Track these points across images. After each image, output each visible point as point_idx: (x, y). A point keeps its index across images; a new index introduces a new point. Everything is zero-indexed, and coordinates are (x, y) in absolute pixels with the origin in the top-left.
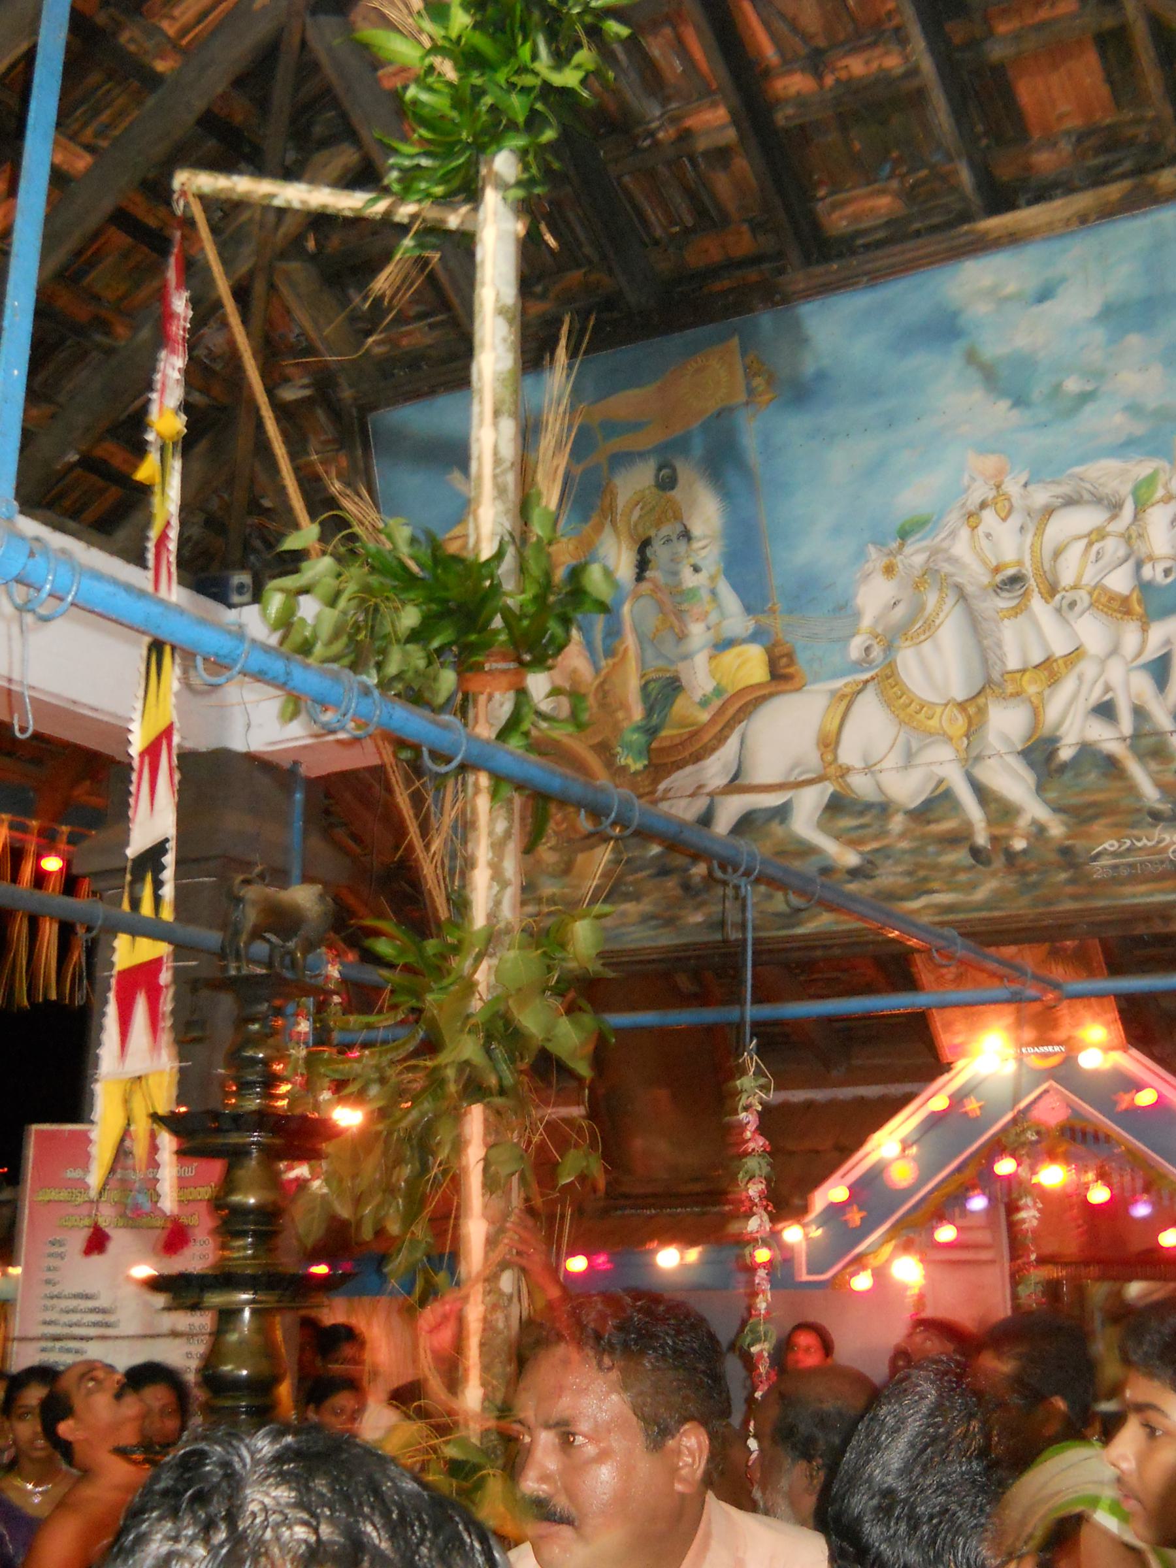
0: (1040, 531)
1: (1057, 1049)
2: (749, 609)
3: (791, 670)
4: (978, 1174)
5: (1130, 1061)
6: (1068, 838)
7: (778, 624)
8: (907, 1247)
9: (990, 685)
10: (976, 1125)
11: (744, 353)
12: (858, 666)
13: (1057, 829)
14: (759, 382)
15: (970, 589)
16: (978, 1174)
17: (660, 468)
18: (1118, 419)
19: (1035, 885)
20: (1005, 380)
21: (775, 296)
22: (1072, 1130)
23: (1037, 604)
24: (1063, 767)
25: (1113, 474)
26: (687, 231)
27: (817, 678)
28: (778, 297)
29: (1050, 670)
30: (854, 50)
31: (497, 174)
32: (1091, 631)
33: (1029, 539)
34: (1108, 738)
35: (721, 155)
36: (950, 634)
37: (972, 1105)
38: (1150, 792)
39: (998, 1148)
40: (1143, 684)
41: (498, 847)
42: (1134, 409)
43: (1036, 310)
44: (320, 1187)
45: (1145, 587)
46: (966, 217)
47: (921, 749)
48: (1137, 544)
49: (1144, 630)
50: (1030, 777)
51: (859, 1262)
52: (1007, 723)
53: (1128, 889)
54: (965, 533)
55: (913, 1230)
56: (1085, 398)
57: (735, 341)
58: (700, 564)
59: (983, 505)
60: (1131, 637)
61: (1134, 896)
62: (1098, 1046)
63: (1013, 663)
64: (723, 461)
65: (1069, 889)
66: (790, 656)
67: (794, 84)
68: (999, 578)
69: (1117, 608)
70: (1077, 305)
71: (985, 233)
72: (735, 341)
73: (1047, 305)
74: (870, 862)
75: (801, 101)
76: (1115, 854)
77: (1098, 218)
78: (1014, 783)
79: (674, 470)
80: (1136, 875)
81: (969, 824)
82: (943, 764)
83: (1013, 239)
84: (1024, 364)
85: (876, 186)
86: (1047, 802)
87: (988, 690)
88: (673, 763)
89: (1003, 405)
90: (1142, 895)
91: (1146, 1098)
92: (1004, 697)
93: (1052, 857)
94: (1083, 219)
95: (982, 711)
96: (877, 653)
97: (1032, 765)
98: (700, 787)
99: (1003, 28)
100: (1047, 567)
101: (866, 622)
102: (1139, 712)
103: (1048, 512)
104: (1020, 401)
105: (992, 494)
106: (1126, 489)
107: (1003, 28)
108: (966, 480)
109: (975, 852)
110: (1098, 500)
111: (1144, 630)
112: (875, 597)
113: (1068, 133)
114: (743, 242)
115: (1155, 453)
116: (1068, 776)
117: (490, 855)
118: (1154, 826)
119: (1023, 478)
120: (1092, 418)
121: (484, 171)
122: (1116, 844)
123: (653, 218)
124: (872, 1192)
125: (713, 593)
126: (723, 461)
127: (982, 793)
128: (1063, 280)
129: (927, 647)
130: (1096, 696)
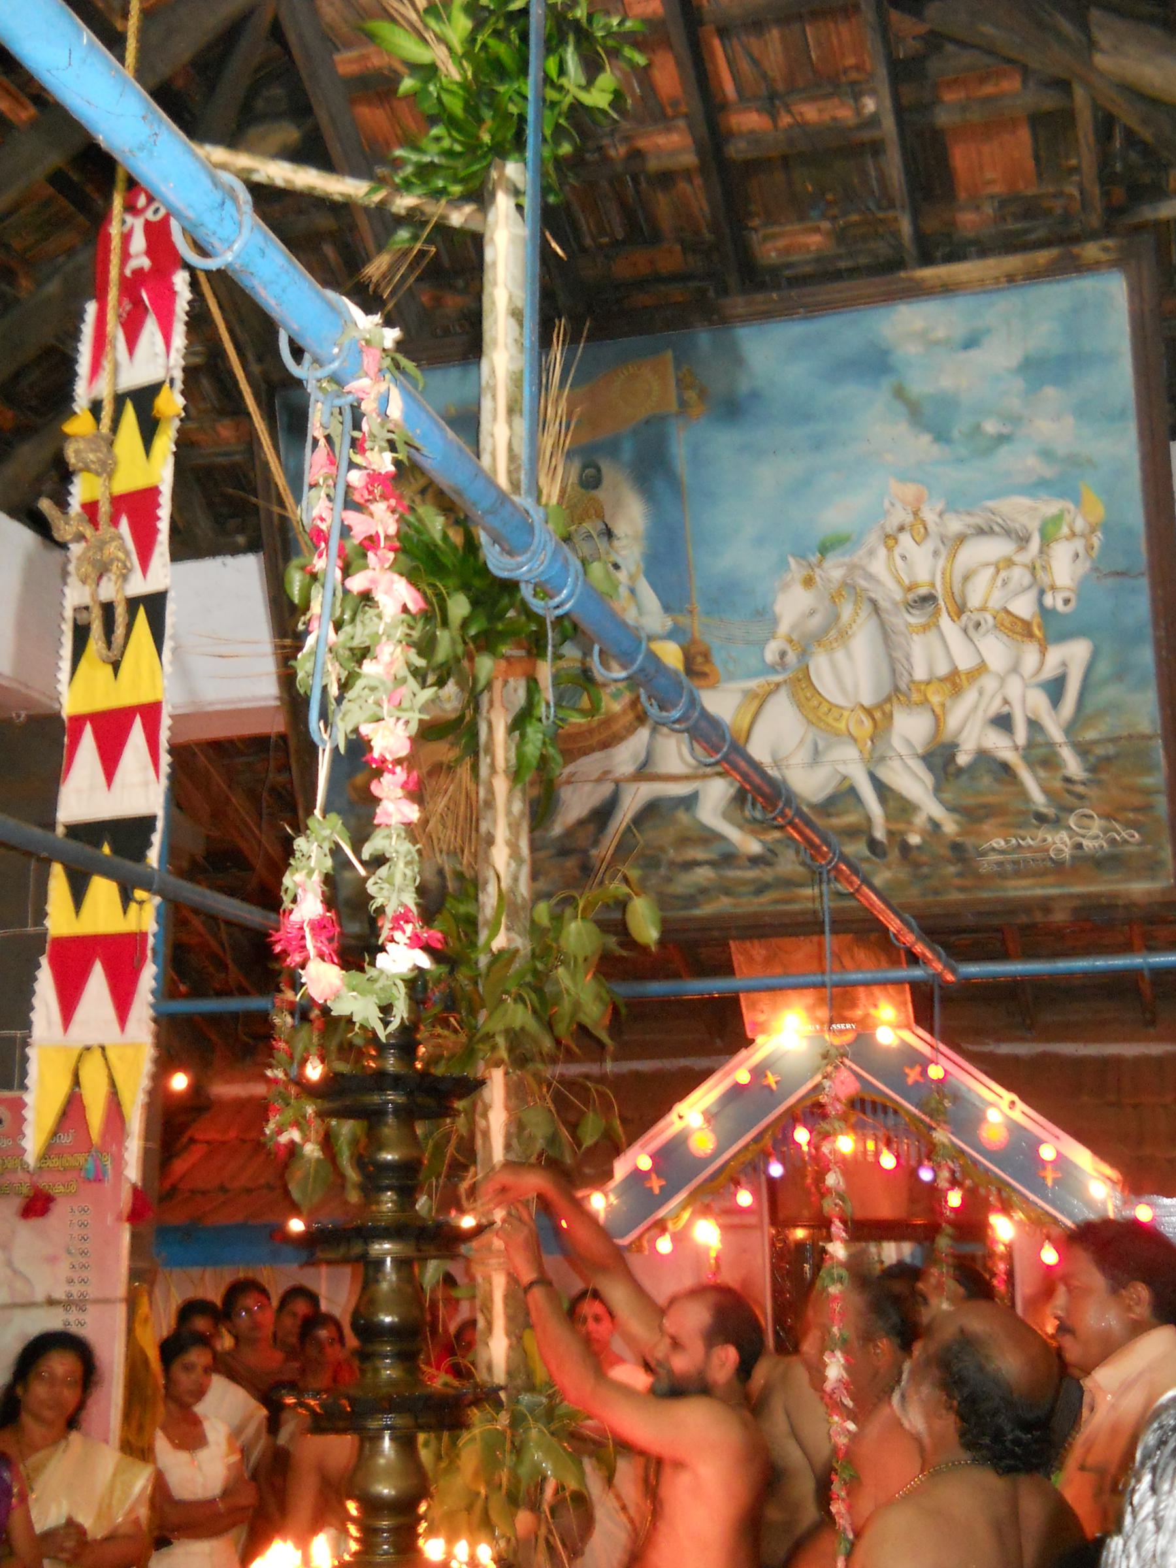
0: (953, 556)
1: (848, 1026)
2: (667, 609)
3: (706, 669)
4: (778, 1140)
5: (917, 1039)
6: (958, 835)
7: (698, 626)
8: (706, 1211)
9: (898, 692)
10: (770, 1096)
11: (678, 367)
12: (772, 669)
13: (950, 827)
14: (691, 395)
15: (884, 604)
16: (778, 1140)
17: (585, 467)
18: (1031, 461)
19: (926, 877)
20: (931, 417)
21: (718, 318)
22: (863, 1101)
23: (945, 621)
24: (960, 771)
25: (1022, 510)
26: (615, 243)
27: (731, 677)
28: (715, 317)
29: (954, 682)
30: (813, 99)
31: (508, 180)
32: (995, 650)
33: (941, 562)
34: (1001, 746)
35: (666, 179)
36: (863, 644)
37: (771, 1080)
38: (1038, 797)
39: (793, 1117)
40: (1039, 701)
41: (513, 827)
42: (1047, 454)
43: (964, 356)
44: (313, 1151)
45: (1045, 612)
46: (895, 264)
47: (829, 747)
48: (1040, 573)
49: (1043, 652)
50: (928, 779)
51: (661, 1227)
52: (911, 728)
53: (1012, 883)
54: (882, 552)
55: (712, 1192)
56: (1002, 439)
57: (669, 355)
58: (620, 561)
59: (901, 529)
60: (1030, 657)
61: (1016, 888)
62: (890, 1024)
63: (920, 674)
64: (652, 468)
65: (957, 881)
66: (706, 656)
67: (748, 121)
68: (911, 596)
69: (1020, 630)
70: (1000, 356)
71: (923, 280)
72: (669, 355)
73: (974, 354)
74: (771, 851)
75: (754, 137)
76: (1002, 852)
77: (1024, 279)
78: (913, 783)
79: (599, 470)
80: (1020, 871)
81: (869, 819)
82: (850, 763)
83: (947, 289)
84: (947, 404)
85: (810, 224)
86: (942, 802)
87: (895, 700)
88: (579, 749)
89: (926, 439)
90: (1024, 888)
91: (935, 1072)
92: (909, 704)
93: (945, 852)
94: (1011, 279)
95: (889, 717)
96: (792, 657)
97: (931, 768)
98: (606, 773)
99: (949, 97)
100: (956, 589)
101: (783, 628)
102: (1034, 725)
103: (961, 539)
104: (941, 436)
105: (908, 519)
106: (1034, 526)
107: (949, 97)
108: (887, 504)
109: (873, 844)
110: (1008, 533)
111: (1043, 652)
112: (793, 605)
113: (992, 197)
114: (670, 258)
115: (1062, 495)
116: (964, 778)
117: (507, 833)
118: (1038, 828)
119: (940, 506)
120: (1005, 457)
121: (494, 175)
122: (1003, 843)
123: (585, 228)
124: (674, 1160)
125: (632, 591)
126: (652, 468)
127: (883, 790)
128: (988, 331)
129: (840, 655)
130: (995, 707)
